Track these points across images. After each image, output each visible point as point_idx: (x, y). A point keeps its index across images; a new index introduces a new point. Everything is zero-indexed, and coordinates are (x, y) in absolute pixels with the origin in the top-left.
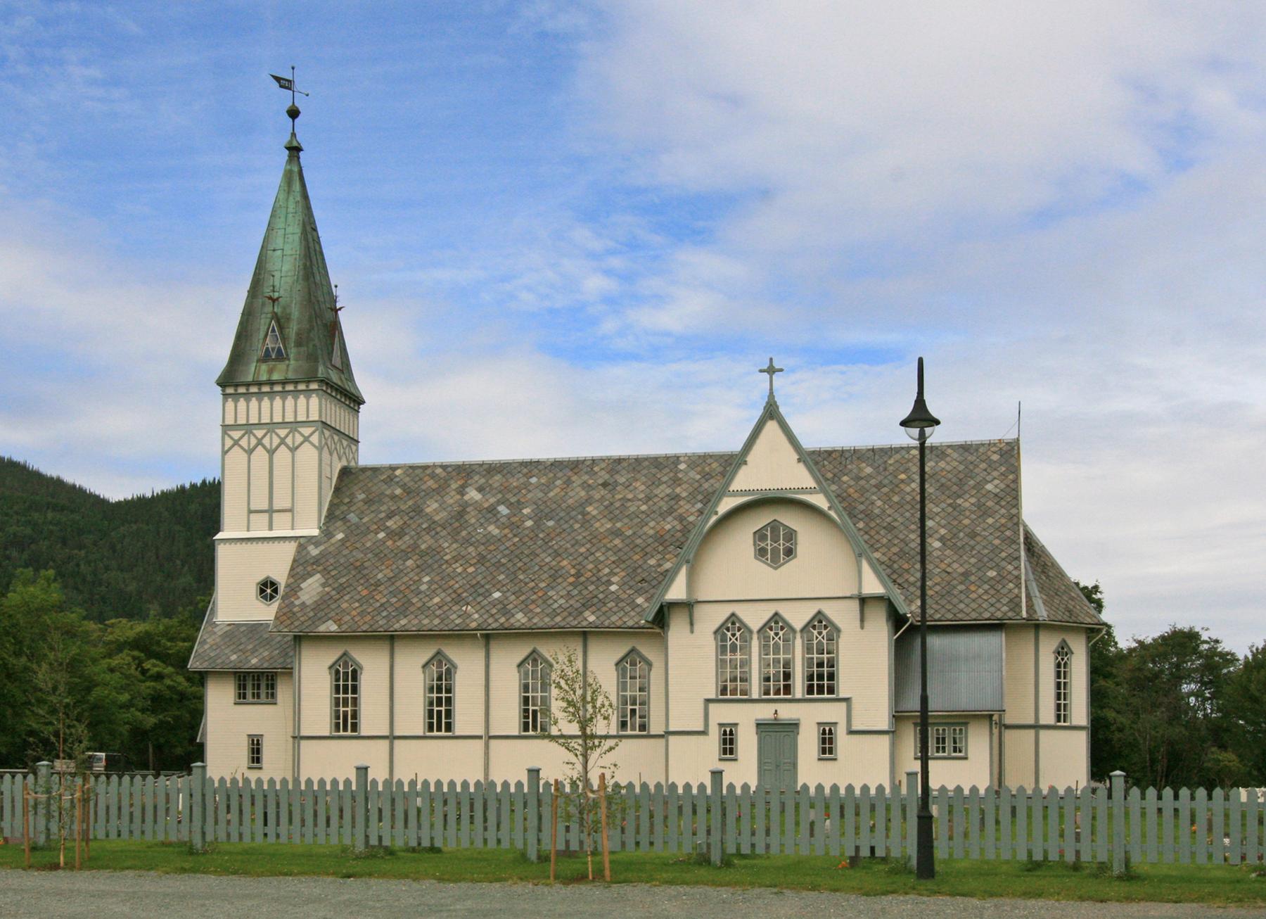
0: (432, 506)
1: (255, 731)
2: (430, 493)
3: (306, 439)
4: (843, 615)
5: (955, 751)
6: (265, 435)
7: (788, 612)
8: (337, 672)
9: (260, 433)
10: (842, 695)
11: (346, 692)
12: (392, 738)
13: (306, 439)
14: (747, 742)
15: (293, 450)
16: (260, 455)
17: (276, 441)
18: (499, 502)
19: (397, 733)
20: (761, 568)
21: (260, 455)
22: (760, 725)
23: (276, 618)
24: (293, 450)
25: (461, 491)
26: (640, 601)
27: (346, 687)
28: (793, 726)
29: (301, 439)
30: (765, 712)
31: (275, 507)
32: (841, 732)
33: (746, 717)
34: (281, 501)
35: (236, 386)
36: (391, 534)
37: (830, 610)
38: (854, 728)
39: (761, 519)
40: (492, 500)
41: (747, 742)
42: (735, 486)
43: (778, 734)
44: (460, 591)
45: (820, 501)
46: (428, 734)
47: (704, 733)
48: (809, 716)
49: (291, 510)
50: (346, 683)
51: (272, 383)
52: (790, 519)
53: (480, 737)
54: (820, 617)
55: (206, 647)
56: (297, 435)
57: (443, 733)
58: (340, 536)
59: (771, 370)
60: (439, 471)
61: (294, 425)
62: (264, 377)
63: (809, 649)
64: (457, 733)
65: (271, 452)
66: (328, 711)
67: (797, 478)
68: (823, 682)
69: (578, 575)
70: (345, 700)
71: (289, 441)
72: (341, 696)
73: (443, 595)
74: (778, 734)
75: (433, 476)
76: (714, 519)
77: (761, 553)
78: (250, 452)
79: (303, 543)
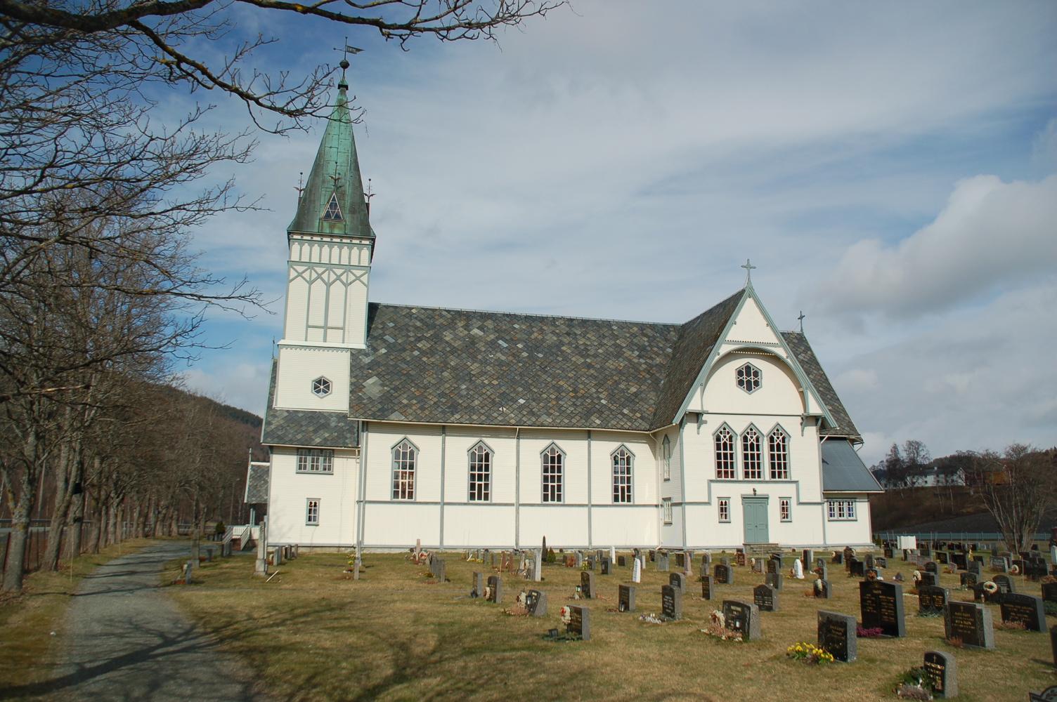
0: (448, 336)
1: (314, 495)
2: (444, 327)
3: (358, 278)
4: (792, 426)
5: (840, 516)
6: (344, 273)
7: (731, 421)
8: (473, 454)
9: (320, 270)
10: (793, 479)
11: (553, 471)
12: (443, 504)
13: (358, 278)
14: (736, 510)
15: (346, 285)
16: (319, 287)
17: (333, 277)
18: (498, 338)
19: (446, 500)
20: (741, 392)
21: (319, 287)
22: (744, 498)
23: (350, 407)
24: (346, 285)
25: (467, 327)
26: (626, 411)
27: (553, 468)
28: (766, 498)
29: (354, 278)
30: (747, 489)
31: (329, 325)
32: (793, 503)
33: (735, 491)
34: (335, 320)
35: (303, 234)
36: (423, 353)
37: (784, 422)
38: (801, 501)
39: (740, 363)
40: (492, 337)
41: (736, 510)
42: (729, 338)
43: (755, 503)
44: (493, 397)
45: (781, 352)
46: (471, 502)
47: (708, 503)
48: (774, 491)
49: (343, 329)
50: (405, 462)
51: (332, 236)
52: (757, 363)
53: (512, 505)
54: (725, 426)
55: (273, 427)
56: (331, 273)
57: (556, 502)
58: (383, 351)
59: (748, 267)
60: (444, 313)
61: (349, 268)
62: (327, 231)
63: (772, 448)
64: (494, 502)
65: (328, 285)
66: (273, 477)
67: (766, 337)
68: (780, 469)
69: (575, 391)
70: (480, 476)
71: (344, 278)
72: (626, 475)
73: (480, 399)
74: (755, 503)
75: (441, 316)
76: (717, 358)
77: (741, 383)
78: (311, 283)
79: (355, 354)
